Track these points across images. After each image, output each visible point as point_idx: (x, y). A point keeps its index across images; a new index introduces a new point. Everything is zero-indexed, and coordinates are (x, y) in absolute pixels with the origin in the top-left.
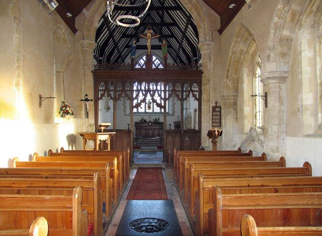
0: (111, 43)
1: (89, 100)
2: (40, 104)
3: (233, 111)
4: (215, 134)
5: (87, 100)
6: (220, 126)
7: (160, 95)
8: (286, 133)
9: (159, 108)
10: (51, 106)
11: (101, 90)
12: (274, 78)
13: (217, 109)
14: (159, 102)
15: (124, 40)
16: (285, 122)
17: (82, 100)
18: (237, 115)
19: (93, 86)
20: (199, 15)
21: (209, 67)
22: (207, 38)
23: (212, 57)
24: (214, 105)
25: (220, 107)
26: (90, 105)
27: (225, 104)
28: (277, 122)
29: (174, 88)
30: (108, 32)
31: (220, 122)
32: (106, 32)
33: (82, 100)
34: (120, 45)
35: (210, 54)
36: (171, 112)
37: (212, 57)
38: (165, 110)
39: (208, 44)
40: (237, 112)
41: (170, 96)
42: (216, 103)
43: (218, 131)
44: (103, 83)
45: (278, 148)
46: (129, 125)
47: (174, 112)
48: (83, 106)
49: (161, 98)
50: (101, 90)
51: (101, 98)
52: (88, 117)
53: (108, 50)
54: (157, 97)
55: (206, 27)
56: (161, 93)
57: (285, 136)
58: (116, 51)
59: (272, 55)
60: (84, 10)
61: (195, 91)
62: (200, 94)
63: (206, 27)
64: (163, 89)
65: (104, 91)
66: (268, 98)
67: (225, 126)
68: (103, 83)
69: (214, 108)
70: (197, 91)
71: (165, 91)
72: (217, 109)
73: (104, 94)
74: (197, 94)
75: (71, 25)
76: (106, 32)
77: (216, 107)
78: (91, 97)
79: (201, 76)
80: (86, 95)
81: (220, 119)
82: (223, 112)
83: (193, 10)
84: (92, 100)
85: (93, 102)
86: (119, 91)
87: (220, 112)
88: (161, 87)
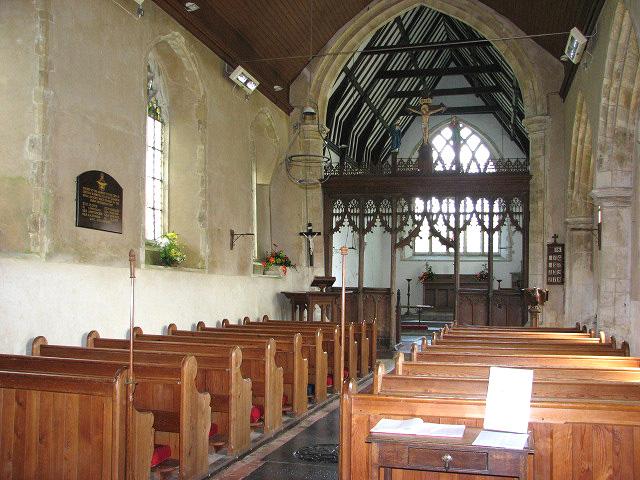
0: (365, 113)
1: (314, 234)
2: (232, 245)
3: (584, 253)
4: (535, 298)
5: (310, 233)
6: (563, 282)
7: (447, 223)
8: (631, 294)
9: (445, 247)
10: (248, 247)
11: (336, 215)
12: (608, 198)
13: (558, 250)
14: (444, 235)
15: (394, 103)
16: (629, 275)
17: (301, 234)
18: (592, 262)
19: (322, 207)
20: (522, 64)
21: (541, 167)
22: (539, 108)
23: (548, 145)
24: (550, 241)
25: (563, 246)
26: (316, 242)
27: (571, 241)
28: (613, 276)
29: (508, 209)
30: (398, 31)
31: (563, 275)
32: (352, 95)
33: (301, 234)
34: (386, 113)
35: (543, 139)
36: (504, 253)
37: (548, 145)
38: (456, 249)
39: (540, 121)
40: (592, 256)
41: (501, 223)
42: (555, 237)
43: (540, 292)
44: (339, 202)
45: (614, 320)
46: (409, 280)
47: (511, 253)
48: (304, 244)
49: (449, 228)
50: (336, 215)
51: (337, 229)
52: (312, 265)
53: (358, 127)
54: (440, 227)
55: (536, 88)
56: (448, 218)
57: (628, 299)
58: (378, 126)
59: (606, 158)
60: (305, 70)
61: (385, 214)
62: (527, 220)
63: (536, 88)
64: (487, 210)
65: (342, 215)
66: (603, 233)
67: (571, 283)
68: (339, 202)
69: (551, 247)
70: (519, 213)
71: (491, 215)
72: (558, 250)
73: (342, 221)
74: (520, 219)
75: (283, 103)
76: (352, 95)
77: (555, 244)
78: (318, 227)
79: (528, 184)
80: (310, 225)
81: (563, 269)
82: (567, 254)
83: (511, 54)
84: (319, 234)
85: (321, 237)
86: (370, 215)
87: (563, 254)
88: (483, 205)
